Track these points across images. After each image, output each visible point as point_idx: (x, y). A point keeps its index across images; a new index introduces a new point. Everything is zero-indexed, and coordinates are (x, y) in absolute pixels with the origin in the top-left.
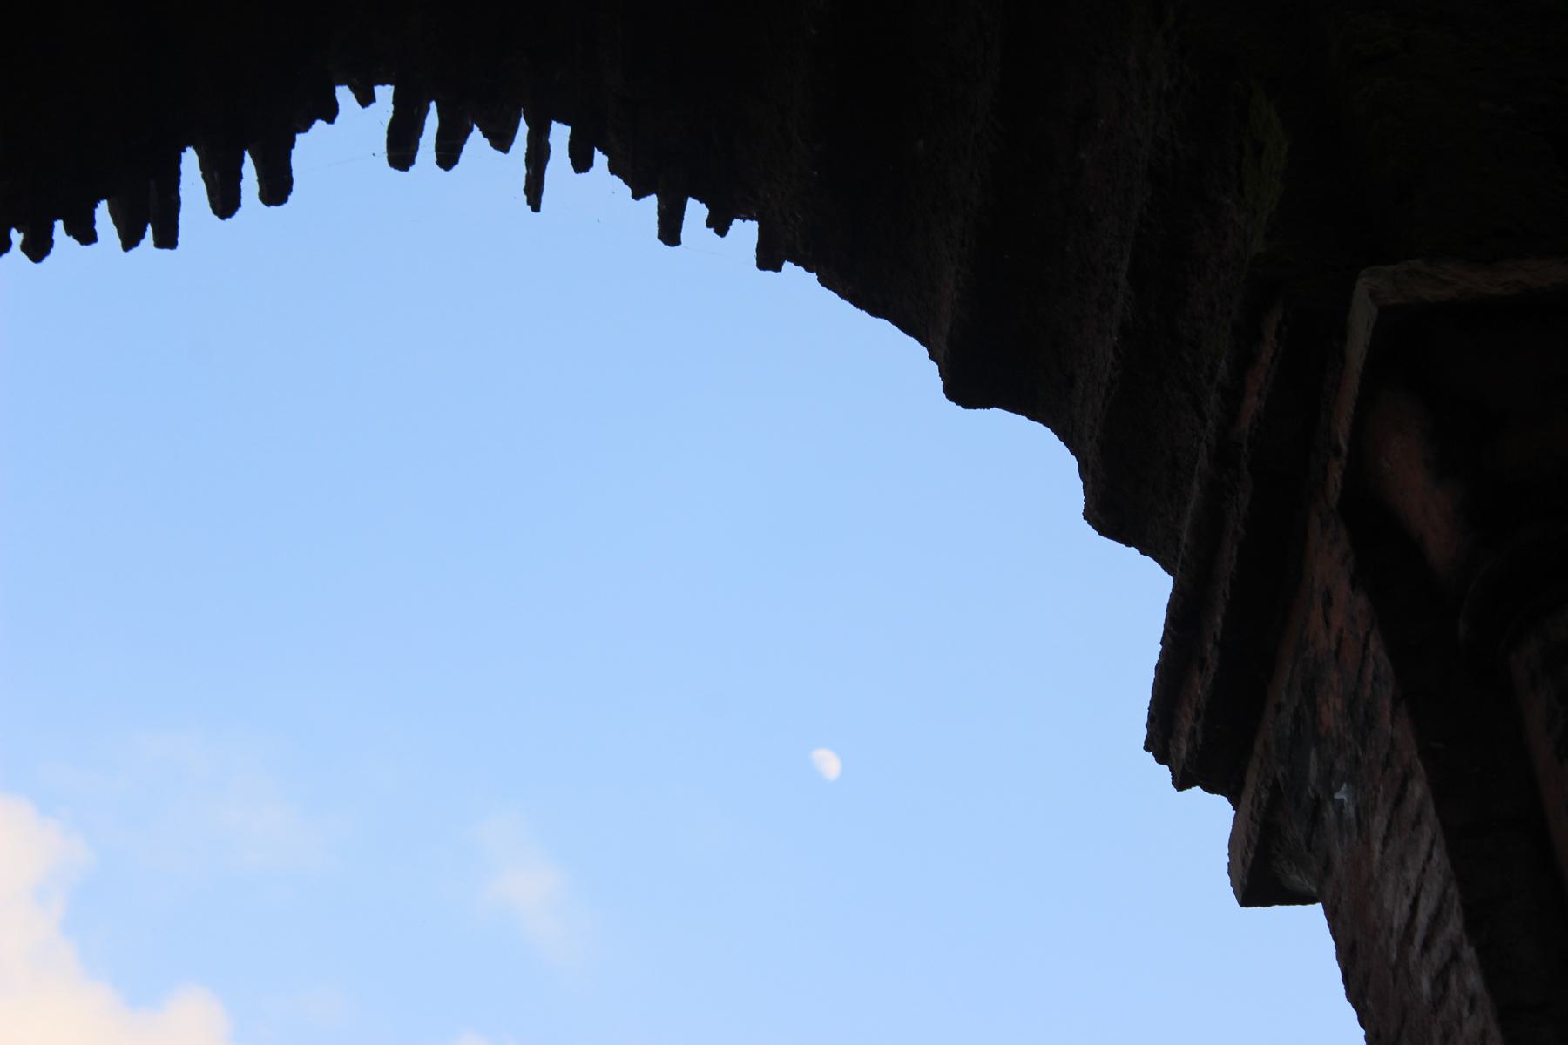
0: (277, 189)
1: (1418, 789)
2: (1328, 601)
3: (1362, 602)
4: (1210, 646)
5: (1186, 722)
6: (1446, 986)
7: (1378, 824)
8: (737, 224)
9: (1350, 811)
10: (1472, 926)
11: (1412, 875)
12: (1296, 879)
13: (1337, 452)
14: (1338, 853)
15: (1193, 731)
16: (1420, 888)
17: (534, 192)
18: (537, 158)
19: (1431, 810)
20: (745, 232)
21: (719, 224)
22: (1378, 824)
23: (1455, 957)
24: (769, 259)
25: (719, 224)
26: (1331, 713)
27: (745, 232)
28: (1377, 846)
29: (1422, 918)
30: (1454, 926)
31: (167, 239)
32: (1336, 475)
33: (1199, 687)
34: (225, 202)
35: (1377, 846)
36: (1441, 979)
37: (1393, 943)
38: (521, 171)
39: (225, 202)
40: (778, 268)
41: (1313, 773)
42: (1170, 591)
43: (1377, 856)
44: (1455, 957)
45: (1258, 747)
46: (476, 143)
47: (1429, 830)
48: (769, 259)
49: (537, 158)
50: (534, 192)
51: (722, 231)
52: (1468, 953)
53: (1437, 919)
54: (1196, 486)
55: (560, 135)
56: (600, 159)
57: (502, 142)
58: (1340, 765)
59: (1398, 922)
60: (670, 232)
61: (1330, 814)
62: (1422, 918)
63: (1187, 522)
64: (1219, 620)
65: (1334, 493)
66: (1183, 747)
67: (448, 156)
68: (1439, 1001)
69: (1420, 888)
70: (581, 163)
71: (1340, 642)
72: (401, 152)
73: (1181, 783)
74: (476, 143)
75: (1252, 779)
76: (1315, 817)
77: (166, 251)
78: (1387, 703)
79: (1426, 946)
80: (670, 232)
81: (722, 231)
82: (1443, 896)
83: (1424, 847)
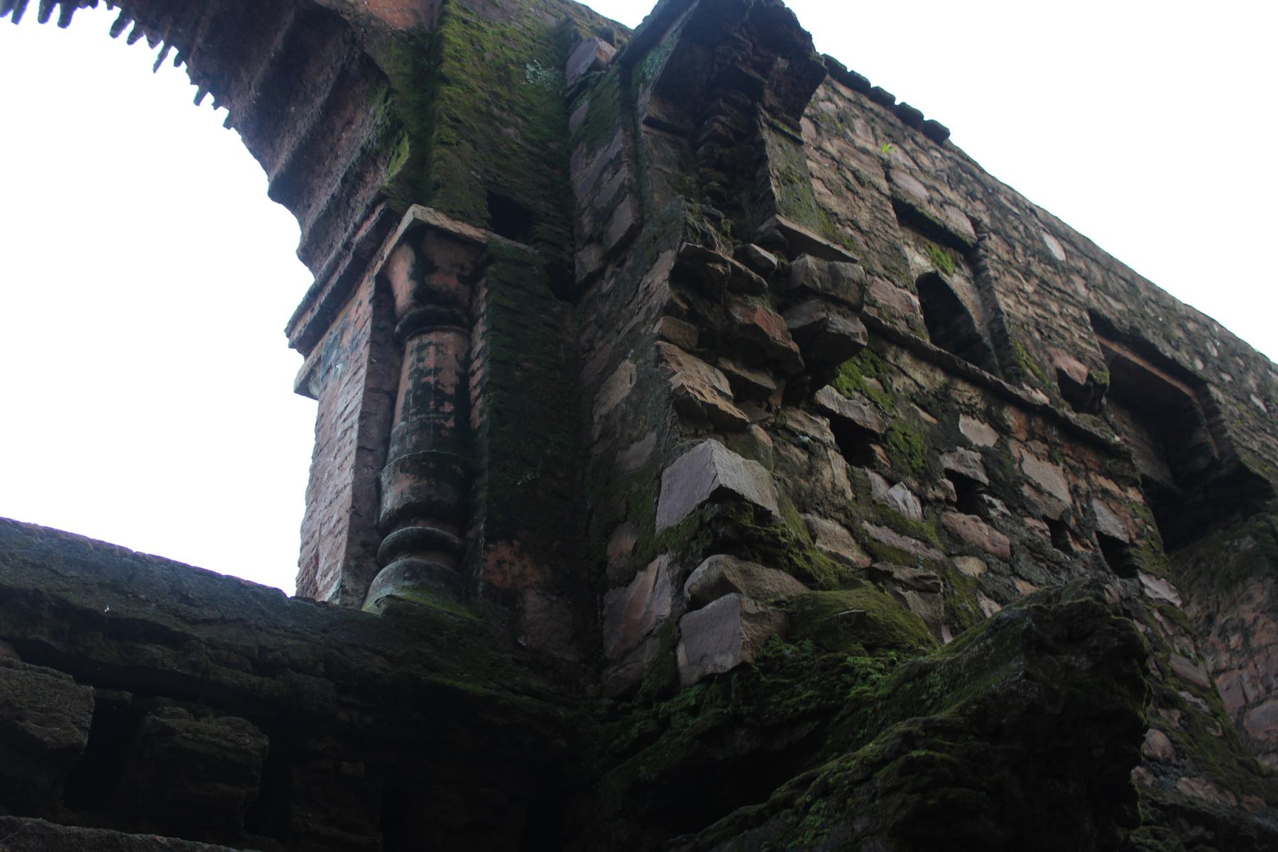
0: (65, 21)
1: (363, 372)
2: (360, 304)
3: (370, 308)
4: (318, 305)
5: (300, 327)
6: (345, 435)
7: (346, 379)
8: (221, 109)
9: (339, 373)
10: (362, 417)
11: (349, 398)
12: (315, 391)
13: (382, 259)
14: (330, 384)
15: (301, 331)
16: (351, 401)
17: (157, 66)
18: (162, 56)
19: (364, 379)
20: (223, 112)
21: (216, 106)
22: (346, 379)
23: (352, 427)
24: (228, 124)
25: (216, 106)
26: (346, 341)
27: (223, 112)
28: (343, 386)
29: (347, 412)
30: (356, 416)
31: (16, 20)
32: (380, 264)
33: (309, 317)
34: (44, 17)
35: (343, 386)
36: (345, 432)
37: (335, 417)
38: (155, 58)
39: (44, 17)
40: (229, 128)
41: (333, 358)
42: (135, 548)
43: (341, 389)
44: (352, 427)
45: (320, 344)
46: (143, 41)
47: (362, 384)
48: (228, 124)
49: (162, 56)
50: (157, 66)
51: (216, 108)
52: (356, 426)
53: (351, 413)
54: (334, 252)
55: (173, 52)
56: (184, 66)
57: (152, 44)
58: (342, 357)
59: (339, 411)
60: (198, 101)
61: (332, 372)
62: (347, 412)
63: (327, 262)
64: (324, 298)
65: (376, 271)
66: (296, 335)
67: (132, 39)
68: (340, 440)
69: (351, 401)
70: (177, 63)
71: (358, 318)
72: (116, 29)
73: (292, 346)
74: (143, 41)
75: (314, 353)
76: (328, 372)
77: (226, 129)
78: (365, 343)
79: (344, 421)
80: (198, 101)
81: (216, 108)
82: (356, 407)
83: (357, 390)
